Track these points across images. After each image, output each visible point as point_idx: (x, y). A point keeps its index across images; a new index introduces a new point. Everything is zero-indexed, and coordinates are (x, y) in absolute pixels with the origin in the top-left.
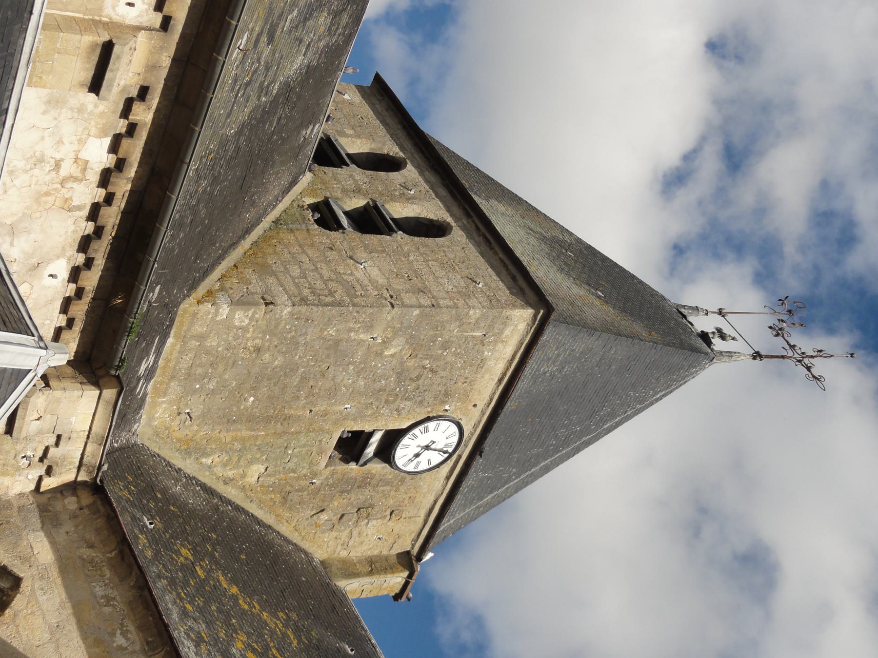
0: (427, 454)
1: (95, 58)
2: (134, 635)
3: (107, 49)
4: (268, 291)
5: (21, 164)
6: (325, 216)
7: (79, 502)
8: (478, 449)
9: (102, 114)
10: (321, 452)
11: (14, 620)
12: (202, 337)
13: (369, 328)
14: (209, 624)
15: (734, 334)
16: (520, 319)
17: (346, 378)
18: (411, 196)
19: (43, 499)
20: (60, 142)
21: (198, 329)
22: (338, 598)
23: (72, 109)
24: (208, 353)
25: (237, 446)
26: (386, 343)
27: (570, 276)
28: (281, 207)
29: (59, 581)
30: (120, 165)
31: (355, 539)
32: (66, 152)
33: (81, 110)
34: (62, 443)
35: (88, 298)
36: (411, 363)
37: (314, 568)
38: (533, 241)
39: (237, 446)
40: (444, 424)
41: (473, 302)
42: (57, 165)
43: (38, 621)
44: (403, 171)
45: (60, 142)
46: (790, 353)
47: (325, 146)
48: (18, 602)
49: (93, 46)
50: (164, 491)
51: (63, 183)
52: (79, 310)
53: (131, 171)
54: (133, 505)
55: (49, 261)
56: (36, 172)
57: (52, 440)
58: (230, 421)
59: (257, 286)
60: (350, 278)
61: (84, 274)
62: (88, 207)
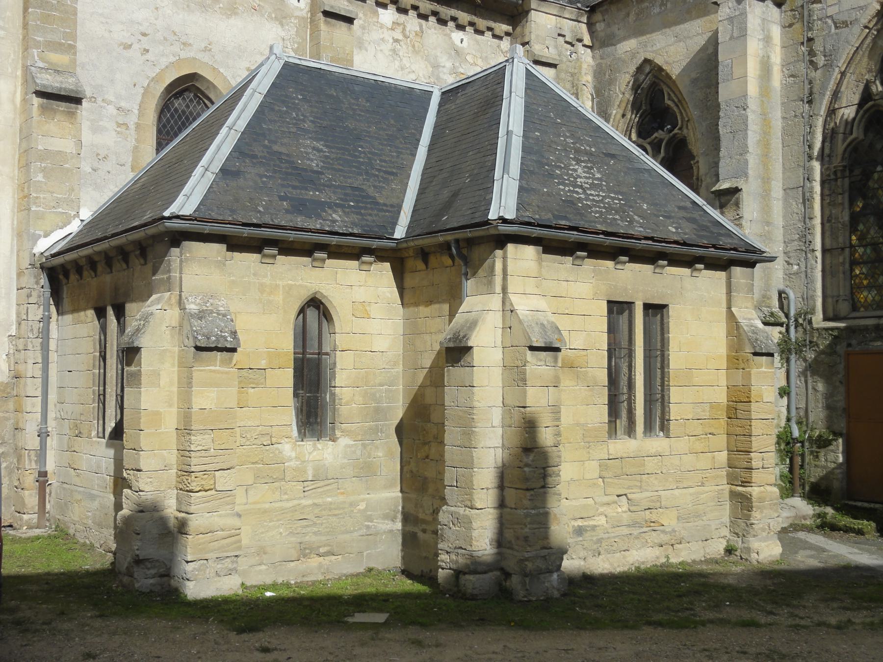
1: (333, 21)
3: (327, 14)
5: (397, 63)
7: (600, 22)
9: (365, 15)
11: (670, 64)
19: (597, 44)
20: (383, 39)
23: (363, 33)
29: (648, 36)
32: (388, 36)
33: (363, 28)
34: (563, 33)
42: (396, 41)
45: (383, 39)
48: (659, 61)
51: (406, 37)
52: (482, 23)
55: (453, 43)
56: (401, 54)
57: (561, 39)
61: (460, 22)
62: (420, 20)
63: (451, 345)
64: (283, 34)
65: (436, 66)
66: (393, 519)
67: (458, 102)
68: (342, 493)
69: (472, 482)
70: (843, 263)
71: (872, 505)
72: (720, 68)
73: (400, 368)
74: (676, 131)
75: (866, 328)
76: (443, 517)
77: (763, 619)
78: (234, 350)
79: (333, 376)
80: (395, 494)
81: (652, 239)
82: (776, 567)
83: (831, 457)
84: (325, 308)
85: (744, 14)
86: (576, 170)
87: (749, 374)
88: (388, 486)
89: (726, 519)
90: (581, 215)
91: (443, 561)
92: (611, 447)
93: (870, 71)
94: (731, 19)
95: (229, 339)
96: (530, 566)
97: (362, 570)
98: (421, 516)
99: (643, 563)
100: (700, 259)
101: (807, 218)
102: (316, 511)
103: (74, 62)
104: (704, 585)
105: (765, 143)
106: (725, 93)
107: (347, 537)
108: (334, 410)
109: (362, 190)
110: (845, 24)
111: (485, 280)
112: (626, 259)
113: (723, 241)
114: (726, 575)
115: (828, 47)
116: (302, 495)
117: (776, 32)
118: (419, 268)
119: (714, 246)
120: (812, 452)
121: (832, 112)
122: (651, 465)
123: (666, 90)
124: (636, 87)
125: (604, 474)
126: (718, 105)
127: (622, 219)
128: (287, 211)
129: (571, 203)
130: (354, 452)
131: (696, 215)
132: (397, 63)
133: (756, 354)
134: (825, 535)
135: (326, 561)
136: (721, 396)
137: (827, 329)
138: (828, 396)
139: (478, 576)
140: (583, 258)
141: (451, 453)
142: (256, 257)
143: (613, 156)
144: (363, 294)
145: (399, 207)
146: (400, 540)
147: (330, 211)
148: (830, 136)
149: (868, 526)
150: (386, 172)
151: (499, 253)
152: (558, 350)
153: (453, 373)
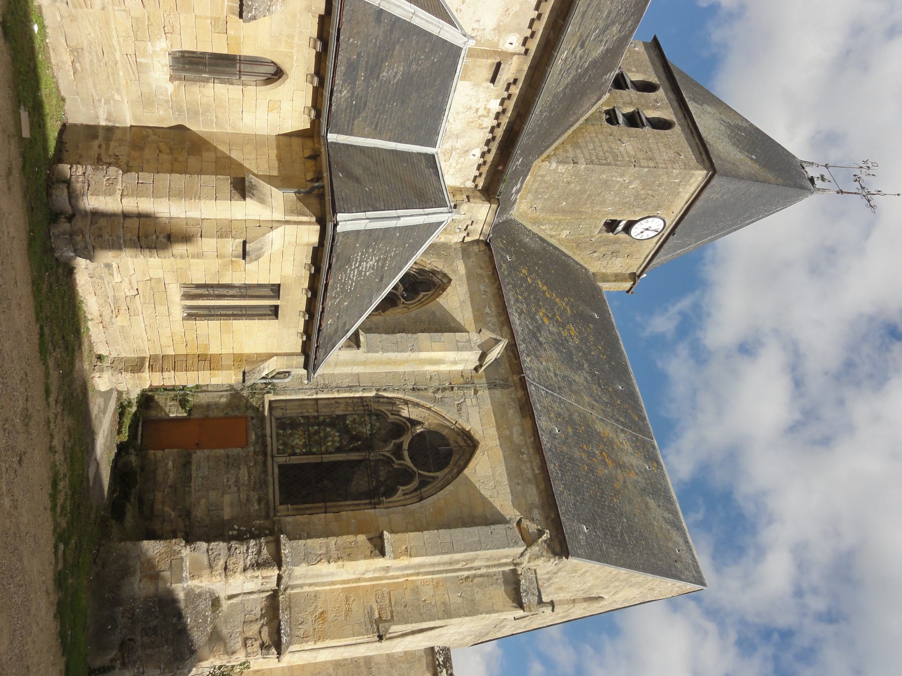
0: (646, 233)
1: (493, 69)
2: (493, 309)
3: (499, 65)
4: (576, 157)
5: (461, 110)
6: (612, 117)
8: (672, 232)
10: (596, 227)
12: (543, 176)
13: (622, 175)
14: (528, 305)
15: (830, 178)
16: (700, 175)
17: (610, 197)
18: (659, 106)
19: (464, 246)
21: (541, 173)
22: (598, 290)
24: (545, 183)
25: (557, 222)
26: (630, 183)
27: (738, 147)
28: (590, 112)
30: (504, 111)
31: (610, 265)
32: (481, 105)
35: (488, 165)
36: (642, 192)
37: (588, 277)
38: (723, 128)
39: (557, 222)
40: (656, 220)
41: (676, 166)
42: (477, 110)
43: (456, 298)
44: (657, 92)
46: (861, 191)
47: (620, 77)
48: (449, 289)
49: (492, 64)
50: (520, 242)
51: (479, 117)
52: (485, 169)
53: (509, 114)
54: (503, 249)
58: (553, 211)
59: (571, 154)
60: (617, 151)
61: (487, 155)
63: (247, 184)
64: (488, 30)
65: (457, 137)
66: (107, 119)
67: (426, 170)
68: (127, 83)
69: (142, 196)
70: (308, 412)
71: (140, 437)
72: (439, 334)
73: (230, 130)
74: (402, 300)
75: (263, 429)
76: (113, 170)
77: (52, 400)
78: (241, 16)
79: (223, 82)
80: (128, 120)
81: (323, 311)
82: (90, 389)
83: (174, 409)
84: (275, 81)
85: (471, 349)
86: (371, 260)
87: (231, 369)
88: (134, 116)
89: (123, 355)
90: (340, 269)
91: (77, 169)
92: (174, 285)
93: (430, 425)
94: (469, 341)
95: (250, 15)
96: (79, 238)
97: (62, 94)
98: (112, 144)
99: (86, 305)
100: (309, 337)
101: (339, 389)
102: (111, 63)
104: (73, 350)
105: (389, 362)
107: (90, 85)
108: (195, 81)
109: (364, 109)
110: (459, 410)
111: (294, 207)
112: (309, 296)
113: (321, 351)
114: (81, 361)
115: (447, 400)
116: (124, 53)
117: (459, 367)
118: (306, 151)
119: (318, 347)
120: (176, 396)
121: (406, 402)
122: (162, 309)
123: (430, 293)
124: (434, 272)
125: (153, 281)
126: (415, 333)
127: (337, 293)
128: (349, 59)
129: (349, 261)
130: (162, 94)
131: (339, 333)
132: (461, 110)
133: (244, 373)
134: (116, 409)
135: (68, 66)
136: (214, 350)
137: (263, 403)
138: (217, 405)
139: (67, 199)
140: (310, 270)
141: (165, 179)
142: (315, 34)
143: (381, 280)
144: (286, 108)
145: (352, 134)
146: (92, 123)
147: (348, 88)
148: (391, 401)
149: (125, 437)
150: (377, 123)
151: (314, 219)
152: (244, 258)
153: (225, 183)
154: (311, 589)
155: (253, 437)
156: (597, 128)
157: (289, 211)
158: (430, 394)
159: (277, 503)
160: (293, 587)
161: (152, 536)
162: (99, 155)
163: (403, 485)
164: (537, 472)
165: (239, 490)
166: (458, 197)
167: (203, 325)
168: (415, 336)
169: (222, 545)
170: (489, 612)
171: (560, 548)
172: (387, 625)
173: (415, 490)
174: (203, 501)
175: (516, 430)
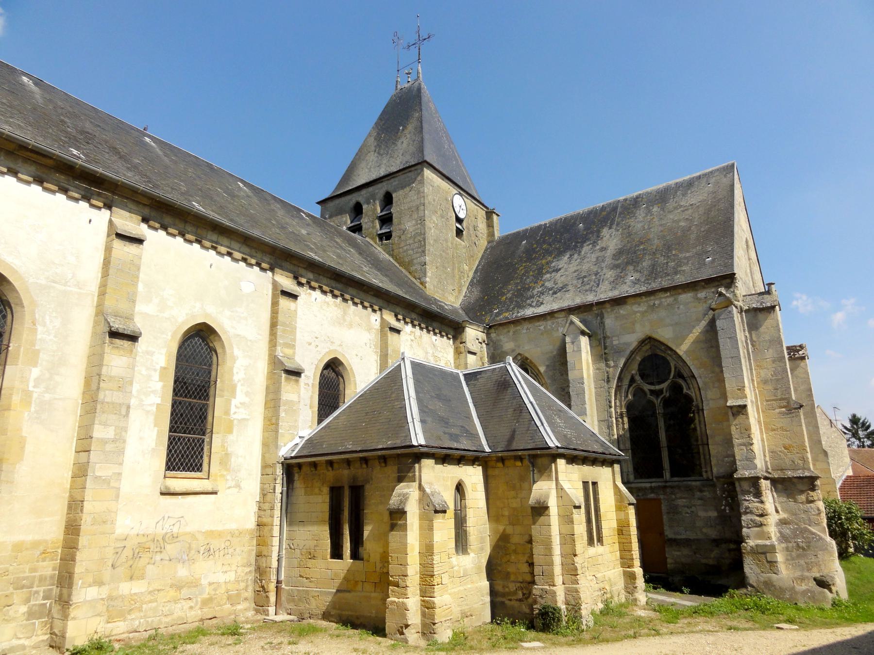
3: (120, 236)
16: (428, 173)
26: (434, 222)
41: (421, 189)
59: (418, 267)
75: (646, 488)
103: (294, 353)
106: (571, 375)
154: (767, 455)
155: (652, 496)
156: (395, 247)
157: (549, 478)
158: (611, 369)
159: (701, 478)
160: (767, 468)
161: (665, 563)
162: (517, 600)
163: (682, 389)
164: (668, 294)
165: (694, 505)
166: (462, 350)
167: (605, 532)
168: (571, 381)
169: (744, 518)
170: (779, 330)
171: (729, 279)
172: (792, 402)
173: (686, 381)
174: (704, 530)
175: (635, 308)
